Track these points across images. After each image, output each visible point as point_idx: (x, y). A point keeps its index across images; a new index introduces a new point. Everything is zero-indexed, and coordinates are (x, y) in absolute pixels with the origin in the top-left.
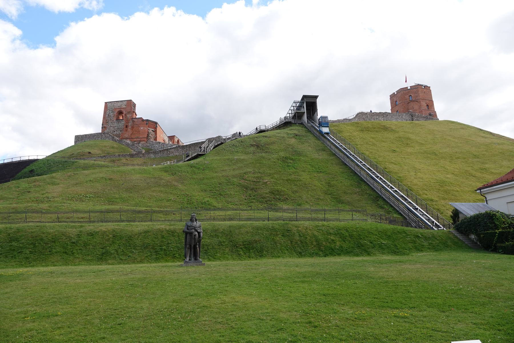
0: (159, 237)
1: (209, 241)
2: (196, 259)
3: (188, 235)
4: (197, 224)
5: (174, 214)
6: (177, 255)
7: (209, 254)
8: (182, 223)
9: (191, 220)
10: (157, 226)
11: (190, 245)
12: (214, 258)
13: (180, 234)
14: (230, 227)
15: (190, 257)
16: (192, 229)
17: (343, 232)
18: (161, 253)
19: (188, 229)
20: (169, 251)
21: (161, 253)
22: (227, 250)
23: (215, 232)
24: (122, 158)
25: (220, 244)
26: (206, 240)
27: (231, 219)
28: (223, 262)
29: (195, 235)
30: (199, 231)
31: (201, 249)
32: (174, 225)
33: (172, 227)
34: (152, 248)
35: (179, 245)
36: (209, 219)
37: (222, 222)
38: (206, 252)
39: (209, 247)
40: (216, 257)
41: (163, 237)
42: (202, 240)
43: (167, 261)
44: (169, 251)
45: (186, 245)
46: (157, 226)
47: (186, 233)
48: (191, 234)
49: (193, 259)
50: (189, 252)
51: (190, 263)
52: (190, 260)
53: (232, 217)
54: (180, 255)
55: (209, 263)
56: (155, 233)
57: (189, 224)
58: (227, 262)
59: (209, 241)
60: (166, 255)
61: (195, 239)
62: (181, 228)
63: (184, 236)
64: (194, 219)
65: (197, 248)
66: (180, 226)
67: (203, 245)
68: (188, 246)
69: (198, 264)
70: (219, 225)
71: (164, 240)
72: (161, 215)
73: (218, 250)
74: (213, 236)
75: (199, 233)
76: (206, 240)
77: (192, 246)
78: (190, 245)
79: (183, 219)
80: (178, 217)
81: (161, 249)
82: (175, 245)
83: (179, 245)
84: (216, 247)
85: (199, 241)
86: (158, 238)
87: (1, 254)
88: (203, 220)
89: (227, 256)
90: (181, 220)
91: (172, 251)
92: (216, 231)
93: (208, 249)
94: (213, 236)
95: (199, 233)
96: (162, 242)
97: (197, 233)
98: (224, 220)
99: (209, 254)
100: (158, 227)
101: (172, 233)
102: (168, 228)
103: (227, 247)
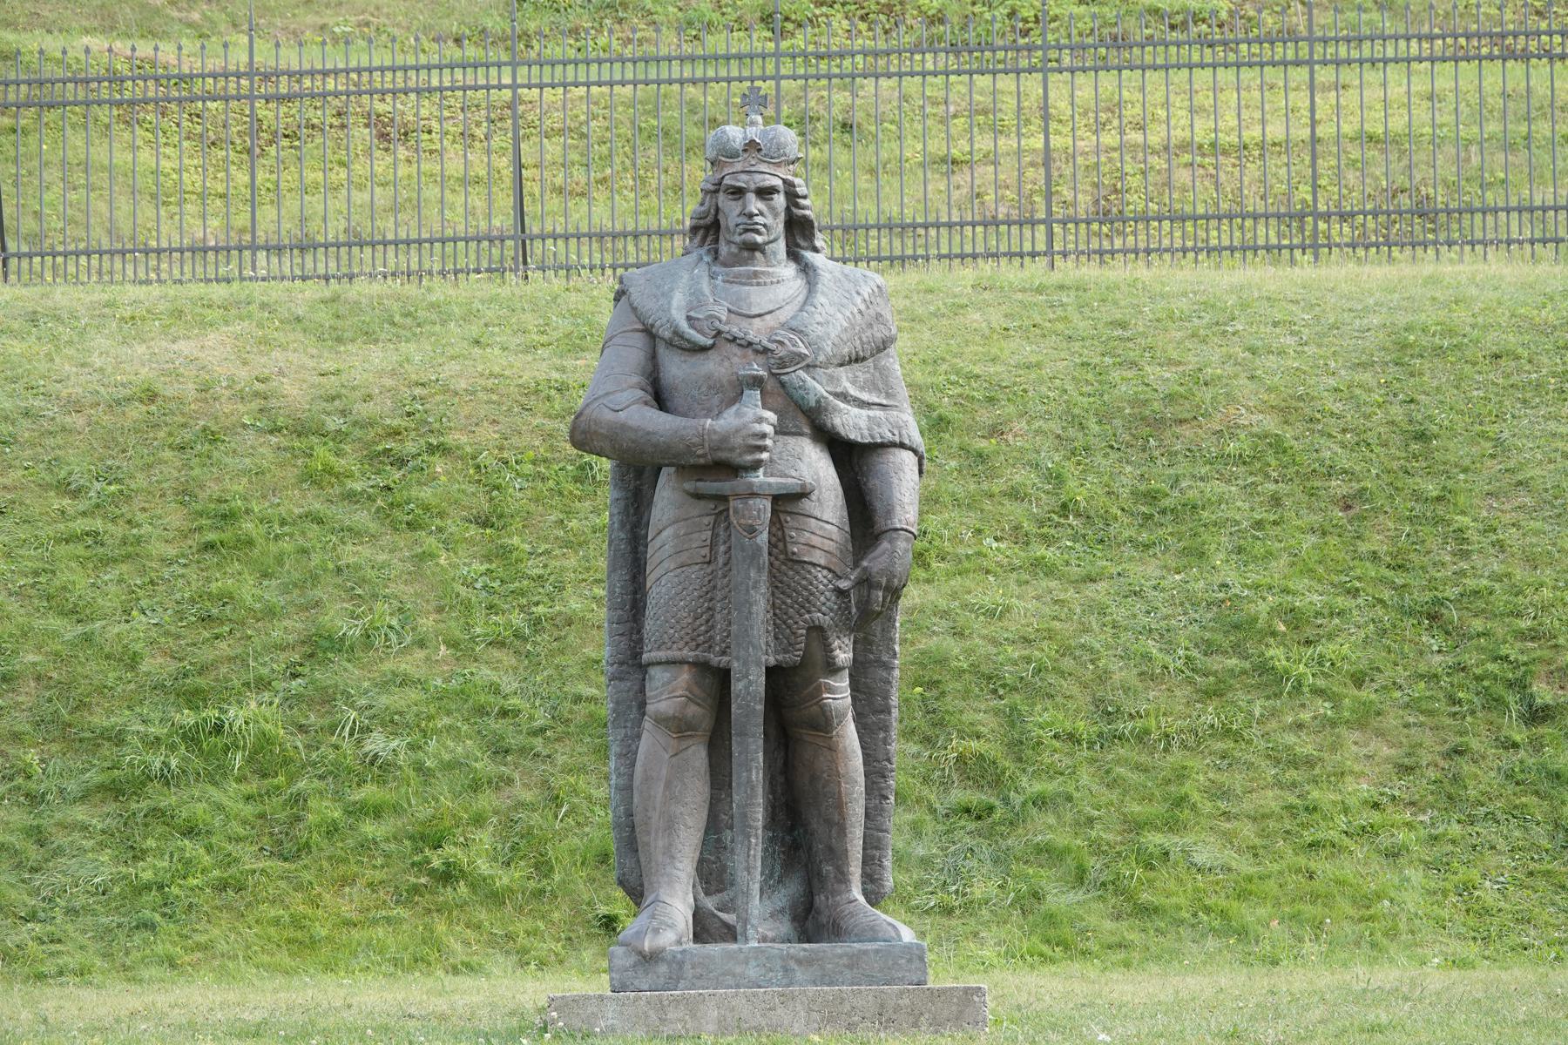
0: (162, 528)
1: (1027, 605)
2: (812, 920)
3: (667, 498)
4: (809, 303)
5: (387, 133)
6: (479, 853)
7: (1047, 829)
8: (542, 285)
9: (708, 229)
10: (103, 348)
11: (717, 682)
12: (1126, 897)
13: (516, 495)
14: (1402, 351)
15: (712, 875)
16: (736, 390)
17: (1099, 919)
18: (195, 803)
19: (660, 397)
20: (335, 773)
21: (195, 803)
22: (1361, 771)
23: (1144, 460)
24: (354, 916)
25: (1239, 656)
26: (990, 593)
27: (1416, 221)
28: (1294, 980)
29: (788, 501)
30: (852, 422)
31: (901, 750)
32: (405, 323)
33: (366, 365)
34: (62, 732)
35: (496, 672)
36: (1028, 222)
37: (1261, 276)
38: (986, 803)
39: (1043, 718)
40: (1168, 890)
41: (220, 533)
42: (912, 596)
43: (303, 945)
44: (335, 773)
45: (632, 663)
46: (103, 348)
47: (639, 471)
48: (717, 469)
49: (760, 910)
50: (696, 792)
51: (706, 976)
52: (704, 928)
53: (1436, 177)
54: (522, 845)
55: (1051, 986)
56: (77, 466)
57: (684, 292)
58: (1360, 974)
59: (1027, 605)
60: (289, 848)
61: (785, 563)
62: (539, 369)
63: (597, 512)
64: (770, 220)
65: (823, 724)
66: (523, 348)
67: (932, 675)
68: (669, 691)
69: (864, 996)
70: (1218, 321)
71: (248, 590)
72: (157, 154)
73: (1201, 771)
74: (1093, 526)
75: (852, 459)
76: (990, 593)
77: (750, 686)
78: (717, 682)
79: (546, 213)
80: (456, 182)
81: (206, 743)
82: (432, 667)
83: (496, 672)
84: (1165, 708)
85: (868, 609)
86: (132, 550)
87: (411, 1043)
88: (900, 241)
89: (1357, 866)
90: (520, 245)
91: (380, 768)
92: (1150, 425)
93: (1018, 747)
94: (1093, 526)
95: (852, 459)
96: (211, 615)
97: (815, 467)
98: (1301, 228)
99: (1047, 829)
100: (138, 362)
101: (385, 460)
102: (296, 373)
103: (1365, 718)
